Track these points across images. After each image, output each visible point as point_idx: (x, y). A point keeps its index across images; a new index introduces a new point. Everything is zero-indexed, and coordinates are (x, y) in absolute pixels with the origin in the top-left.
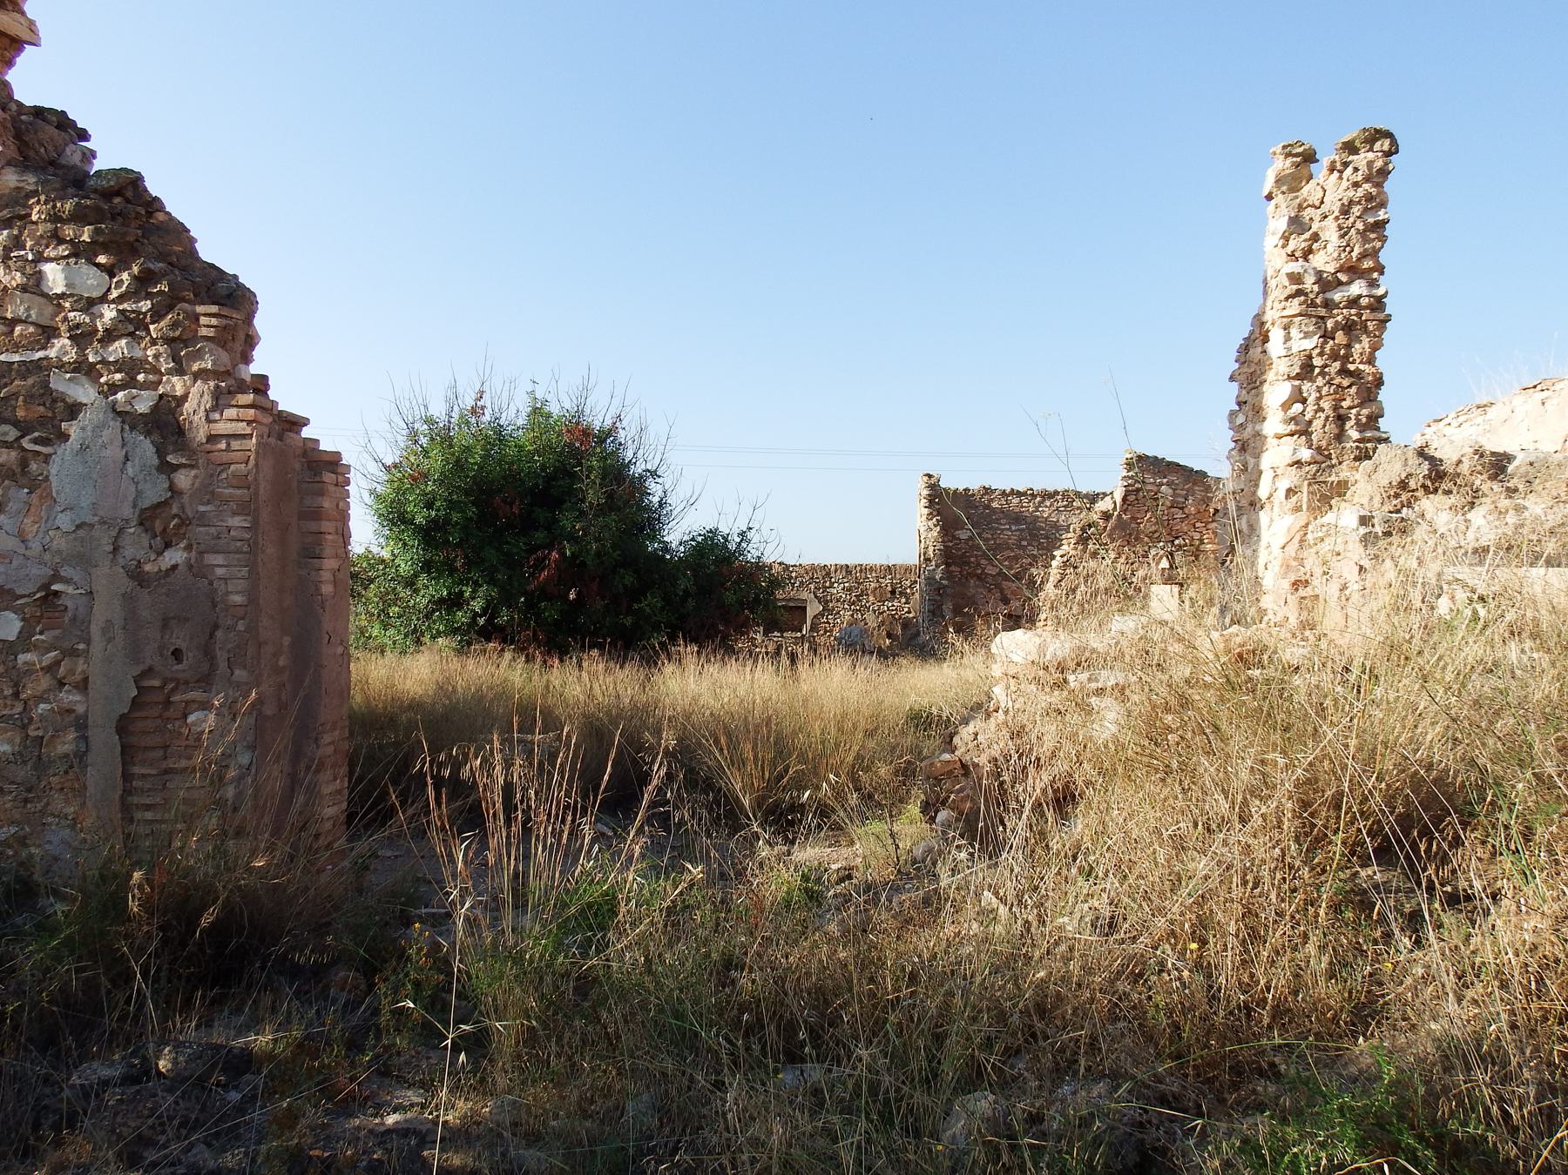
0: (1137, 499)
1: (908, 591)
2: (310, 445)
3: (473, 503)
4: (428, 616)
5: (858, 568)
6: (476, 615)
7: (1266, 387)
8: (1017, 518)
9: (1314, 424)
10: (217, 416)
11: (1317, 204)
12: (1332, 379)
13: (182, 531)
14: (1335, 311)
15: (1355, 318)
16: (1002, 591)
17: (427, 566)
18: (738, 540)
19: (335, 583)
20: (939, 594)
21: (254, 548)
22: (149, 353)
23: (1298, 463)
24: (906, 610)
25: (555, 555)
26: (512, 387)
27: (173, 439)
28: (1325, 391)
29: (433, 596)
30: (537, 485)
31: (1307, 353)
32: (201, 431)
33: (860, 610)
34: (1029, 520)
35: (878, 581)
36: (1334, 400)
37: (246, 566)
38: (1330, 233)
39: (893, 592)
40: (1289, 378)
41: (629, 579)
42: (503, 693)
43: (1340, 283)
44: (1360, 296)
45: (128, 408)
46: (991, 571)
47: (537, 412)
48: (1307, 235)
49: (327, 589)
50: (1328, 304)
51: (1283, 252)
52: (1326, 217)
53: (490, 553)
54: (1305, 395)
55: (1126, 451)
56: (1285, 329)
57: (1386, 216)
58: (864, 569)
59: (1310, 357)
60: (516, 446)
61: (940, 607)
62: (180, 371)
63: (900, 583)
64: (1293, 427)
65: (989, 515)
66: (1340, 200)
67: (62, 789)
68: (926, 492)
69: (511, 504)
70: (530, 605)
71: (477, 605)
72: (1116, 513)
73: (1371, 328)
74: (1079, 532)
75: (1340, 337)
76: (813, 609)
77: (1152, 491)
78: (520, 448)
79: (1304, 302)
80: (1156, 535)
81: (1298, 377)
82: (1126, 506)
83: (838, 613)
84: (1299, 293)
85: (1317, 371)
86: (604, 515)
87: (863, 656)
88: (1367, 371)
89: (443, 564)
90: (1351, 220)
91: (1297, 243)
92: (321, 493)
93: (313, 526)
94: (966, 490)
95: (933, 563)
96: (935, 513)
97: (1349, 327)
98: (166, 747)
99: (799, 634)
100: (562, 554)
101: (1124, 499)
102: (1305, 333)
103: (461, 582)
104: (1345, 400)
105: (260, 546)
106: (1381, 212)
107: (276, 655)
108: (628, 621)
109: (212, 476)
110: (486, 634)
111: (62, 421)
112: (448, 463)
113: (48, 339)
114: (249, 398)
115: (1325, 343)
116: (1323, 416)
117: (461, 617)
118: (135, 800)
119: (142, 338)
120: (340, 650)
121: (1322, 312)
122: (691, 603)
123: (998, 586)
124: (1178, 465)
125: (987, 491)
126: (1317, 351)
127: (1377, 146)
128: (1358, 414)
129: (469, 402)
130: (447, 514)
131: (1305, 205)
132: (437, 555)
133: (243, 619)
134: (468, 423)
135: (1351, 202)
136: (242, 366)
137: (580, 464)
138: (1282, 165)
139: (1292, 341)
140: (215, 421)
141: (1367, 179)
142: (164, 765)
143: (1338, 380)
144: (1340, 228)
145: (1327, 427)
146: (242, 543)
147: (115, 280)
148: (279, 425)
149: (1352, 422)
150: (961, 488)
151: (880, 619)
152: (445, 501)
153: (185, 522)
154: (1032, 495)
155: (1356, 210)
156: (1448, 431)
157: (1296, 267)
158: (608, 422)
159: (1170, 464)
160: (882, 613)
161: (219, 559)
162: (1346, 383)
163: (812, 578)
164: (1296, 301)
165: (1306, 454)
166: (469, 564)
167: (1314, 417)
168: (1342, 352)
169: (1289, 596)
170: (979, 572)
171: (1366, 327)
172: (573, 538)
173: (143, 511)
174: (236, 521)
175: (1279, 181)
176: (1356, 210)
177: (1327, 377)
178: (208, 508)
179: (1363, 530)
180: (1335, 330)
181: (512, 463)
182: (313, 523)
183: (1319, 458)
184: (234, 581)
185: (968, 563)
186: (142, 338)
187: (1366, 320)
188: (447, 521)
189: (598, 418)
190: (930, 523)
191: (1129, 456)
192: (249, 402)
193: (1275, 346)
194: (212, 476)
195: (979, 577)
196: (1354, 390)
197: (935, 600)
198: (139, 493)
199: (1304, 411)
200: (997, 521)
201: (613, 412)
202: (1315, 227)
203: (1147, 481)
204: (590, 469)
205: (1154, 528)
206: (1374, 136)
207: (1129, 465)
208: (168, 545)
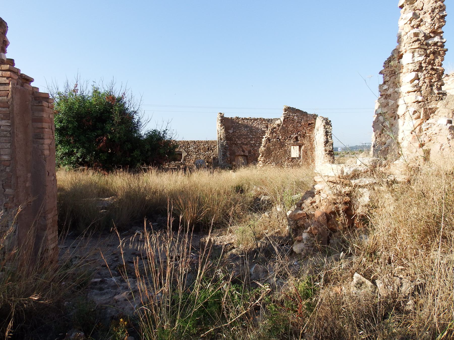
0: (287, 120)
1: (213, 148)
2: (35, 90)
3: (76, 121)
4: (62, 159)
5: (198, 142)
6: (78, 158)
7: (401, 75)
8: (246, 126)
9: (422, 87)
11: (420, 9)
12: (429, 71)
14: (429, 47)
15: (436, 50)
16: (242, 148)
17: (61, 142)
18: (163, 133)
19: (50, 150)
20: (225, 149)
21: (12, 134)
23: (418, 102)
24: (212, 154)
25: (105, 138)
26: (87, 83)
28: (426, 76)
29: (63, 152)
30: (97, 115)
31: (420, 62)
33: (198, 155)
34: (250, 127)
35: (204, 146)
36: (429, 79)
37: (9, 143)
38: (427, 19)
39: (208, 149)
40: (414, 71)
41: (129, 146)
42: (91, 185)
44: (438, 42)
47: (96, 91)
48: (419, 19)
49: (47, 152)
50: (427, 44)
51: (410, 26)
52: (426, 13)
53: (82, 138)
54: (419, 77)
55: (284, 106)
56: (413, 53)
57: (446, 14)
58: (199, 142)
59: (421, 63)
60: (89, 103)
61: (226, 153)
63: (210, 146)
64: (415, 89)
66: (431, 7)
68: (220, 118)
69: (89, 122)
70: (97, 154)
71: (79, 155)
72: (281, 125)
73: (441, 54)
74: (271, 130)
75: (432, 56)
76: (184, 154)
77: (292, 118)
78: (91, 103)
79: (420, 43)
80: (293, 131)
81: (417, 71)
82: (284, 122)
83: (192, 155)
84: (418, 40)
85: (424, 68)
86: (121, 125)
88: (440, 69)
89: (66, 141)
90: (435, 14)
91: (414, 22)
92: (43, 111)
93: (39, 125)
94: (231, 118)
95: (223, 140)
96: (223, 125)
97: (434, 53)
99: (180, 162)
100: (108, 138)
101: (284, 120)
102: (420, 55)
103: (73, 147)
104: (433, 79)
105: (15, 134)
106: (444, 12)
107: (25, 182)
108: (129, 159)
110: (81, 164)
112: (67, 108)
114: (7, 67)
115: (426, 58)
116: (426, 85)
117: (73, 159)
120: (53, 178)
121: (426, 47)
122: (149, 153)
123: (241, 147)
124: (299, 110)
125: (238, 118)
126: (424, 61)
129: (72, 88)
130: (67, 125)
131: (416, 9)
132: (64, 138)
133: (9, 166)
134: (73, 95)
135: (435, 8)
136: (2, 54)
137: (112, 109)
139: (415, 58)
143: (430, 72)
144: (431, 17)
145: (427, 89)
146: (7, 132)
148: (21, 80)
149: (435, 87)
150: (230, 118)
151: (205, 157)
152: (66, 120)
154: (251, 119)
155: (437, 11)
157: (416, 30)
158: (121, 95)
159: (297, 110)
160: (205, 155)
162: (433, 73)
163: (184, 145)
164: (417, 43)
166: (75, 141)
167: (423, 85)
168: (432, 62)
169: (418, 150)
170: (236, 142)
171: (440, 53)
172: (110, 133)
176: (437, 11)
177: (427, 71)
179: (449, 125)
180: (430, 54)
181: (89, 108)
182: (39, 124)
184: (4, 149)
185: (232, 140)
187: (440, 51)
188: (67, 127)
189: (117, 95)
190: (221, 128)
191: (285, 107)
192: (7, 69)
193: (407, 59)
195: (235, 144)
196: (436, 75)
197: (224, 151)
199: (419, 83)
200: (241, 127)
201: (122, 92)
202: (421, 16)
203: (290, 115)
204: (116, 110)
205: (292, 129)
207: (285, 110)
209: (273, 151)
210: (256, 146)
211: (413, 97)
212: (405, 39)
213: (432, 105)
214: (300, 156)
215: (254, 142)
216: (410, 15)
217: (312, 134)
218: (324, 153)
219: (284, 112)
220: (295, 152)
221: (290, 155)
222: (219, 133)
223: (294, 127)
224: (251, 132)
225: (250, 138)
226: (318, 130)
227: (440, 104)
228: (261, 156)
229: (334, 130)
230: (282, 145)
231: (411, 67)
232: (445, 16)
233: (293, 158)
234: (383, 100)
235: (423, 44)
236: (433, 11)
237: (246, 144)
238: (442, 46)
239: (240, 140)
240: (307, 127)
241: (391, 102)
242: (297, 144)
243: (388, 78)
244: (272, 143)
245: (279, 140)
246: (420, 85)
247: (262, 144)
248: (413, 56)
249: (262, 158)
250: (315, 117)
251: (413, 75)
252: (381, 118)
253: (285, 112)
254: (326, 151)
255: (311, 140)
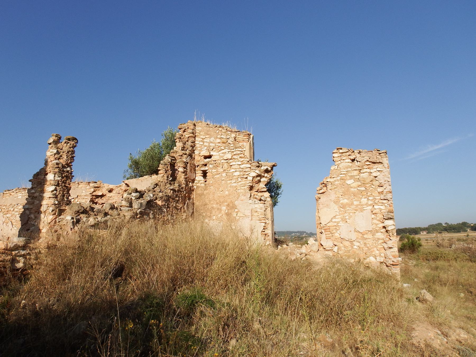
7: (45, 186)
11: (61, 149)
44: (69, 171)
50: (63, 171)
59: (59, 181)
85: (60, 185)
97: (67, 176)
116: (60, 195)
127: (74, 141)
128: (67, 195)
144: (67, 156)
155: (70, 153)
156: (12, 194)
162: (65, 188)
165: (57, 202)
167: (58, 195)
175: (54, 141)
176: (70, 153)
183: (59, 204)
196: (66, 190)
202: (61, 154)
206: (74, 139)
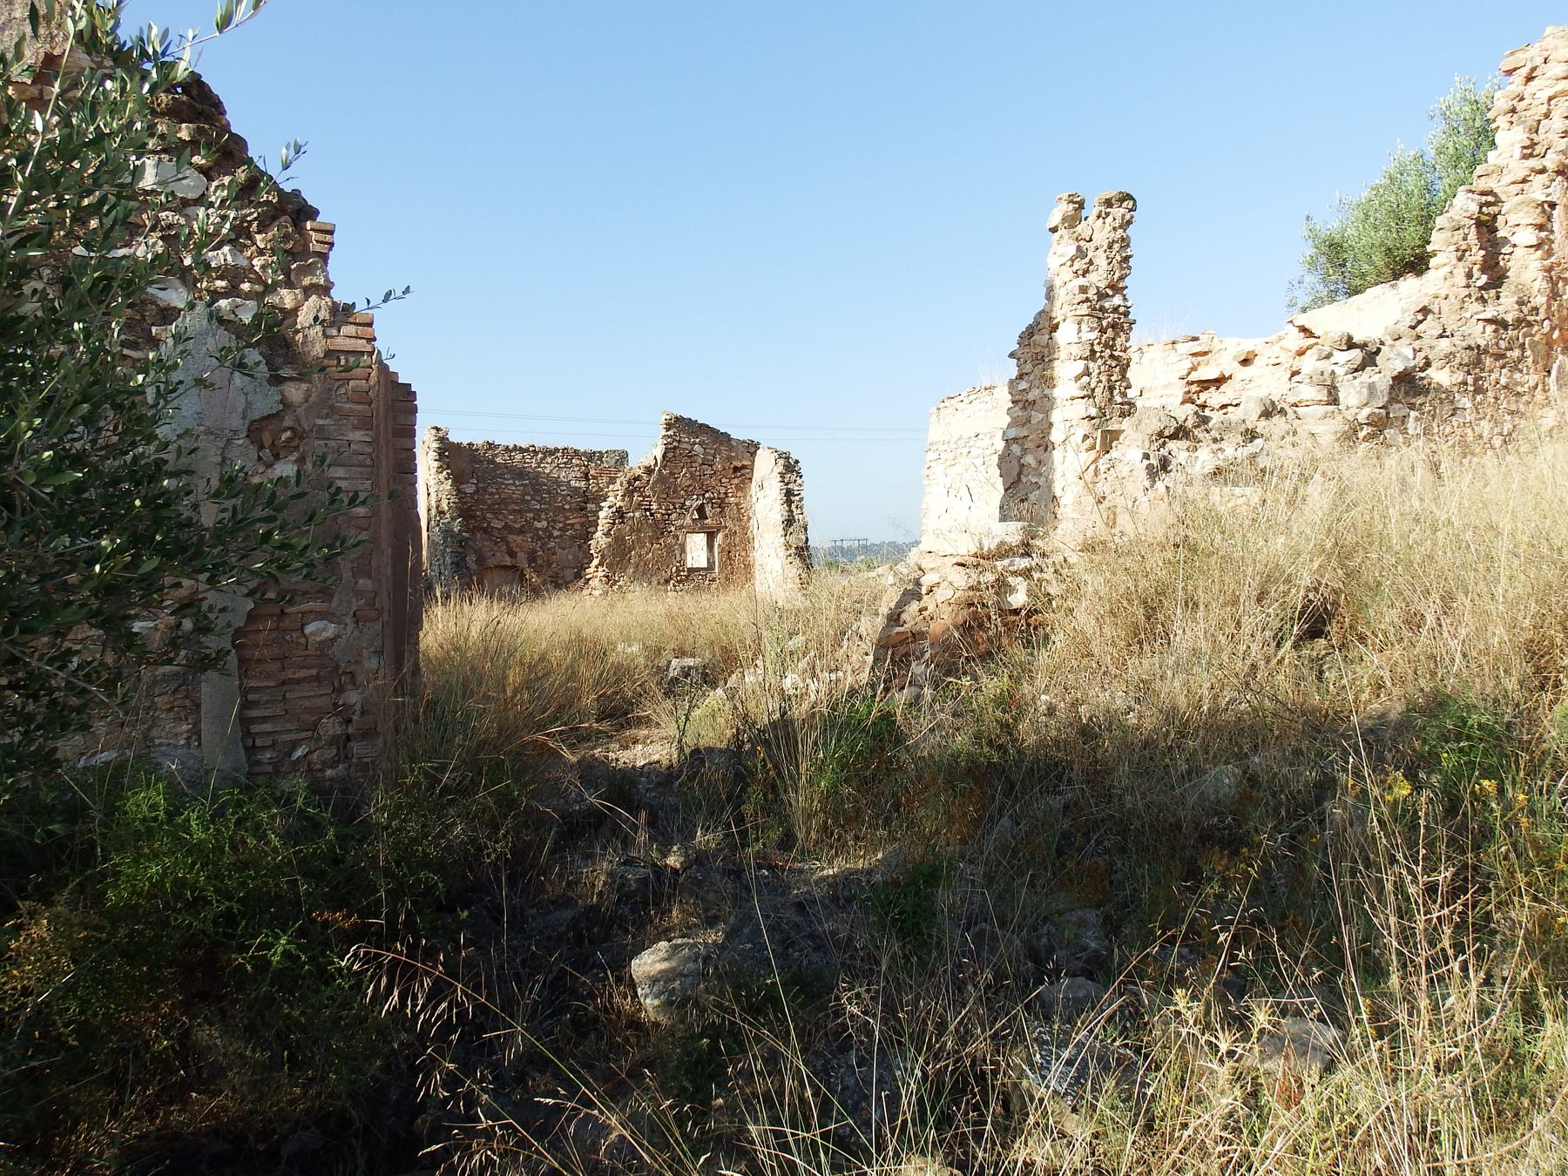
7: (1056, 363)
8: (520, 473)
10: (334, 332)
13: (293, 444)
16: (507, 543)
20: (461, 546)
22: (255, 262)
27: (281, 352)
32: (318, 346)
34: (531, 476)
38: (1101, 261)
43: (1108, 295)
45: (232, 317)
46: (497, 524)
50: (1102, 309)
59: (1092, 345)
62: (289, 284)
64: (1085, 393)
65: (494, 470)
67: (171, 709)
68: (435, 445)
75: (1110, 332)
84: (1087, 300)
87: (499, 600)
91: (1079, 265)
97: (1113, 326)
98: (283, 658)
101: (664, 456)
109: (330, 390)
111: (153, 324)
113: (132, 236)
118: (254, 713)
119: (245, 246)
125: (491, 446)
138: (1066, 208)
140: (333, 337)
141: (1120, 227)
142: (283, 676)
147: (215, 184)
150: (465, 443)
153: (298, 435)
155: (1116, 246)
161: (340, 472)
164: (1086, 305)
173: (252, 422)
174: (357, 436)
175: (1064, 220)
176: (1116, 246)
178: (327, 422)
179: (1146, 462)
180: (1107, 327)
185: (474, 517)
186: (245, 246)
194: (330, 390)
195: (485, 531)
198: (249, 404)
200: (501, 476)
202: (1090, 255)
205: (688, 483)
207: (669, 426)
208: (277, 457)
209: (634, 548)
210: (551, 536)
211: (1083, 408)
212: (1062, 295)
213: (1113, 426)
214: (710, 567)
215: (545, 523)
216: (1072, 251)
217: (745, 497)
218: (782, 553)
219: (664, 433)
220: (696, 551)
221: (682, 561)
222: (433, 495)
223: (693, 477)
224: (537, 492)
225: (531, 511)
226: (761, 487)
227: (1126, 424)
228: (596, 562)
229: (809, 489)
230: (660, 529)
231: (1076, 350)
232: (1130, 257)
233: (691, 570)
234: (1018, 412)
235: (1095, 309)
236: (1110, 247)
237: (521, 531)
238: (1126, 314)
239: (501, 517)
240: (731, 479)
241: (1037, 417)
242: (702, 528)
243: (1028, 368)
244: (630, 522)
245: (652, 515)
246: (1092, 386)
247: (599, 528)
248: (1080, 331)
249: (600, 569)
250: (752, 448)
251: (1080, 366)
252: (1016, 449)
253: (668, 430)
254: (788, 546)
255: (742, 517)
